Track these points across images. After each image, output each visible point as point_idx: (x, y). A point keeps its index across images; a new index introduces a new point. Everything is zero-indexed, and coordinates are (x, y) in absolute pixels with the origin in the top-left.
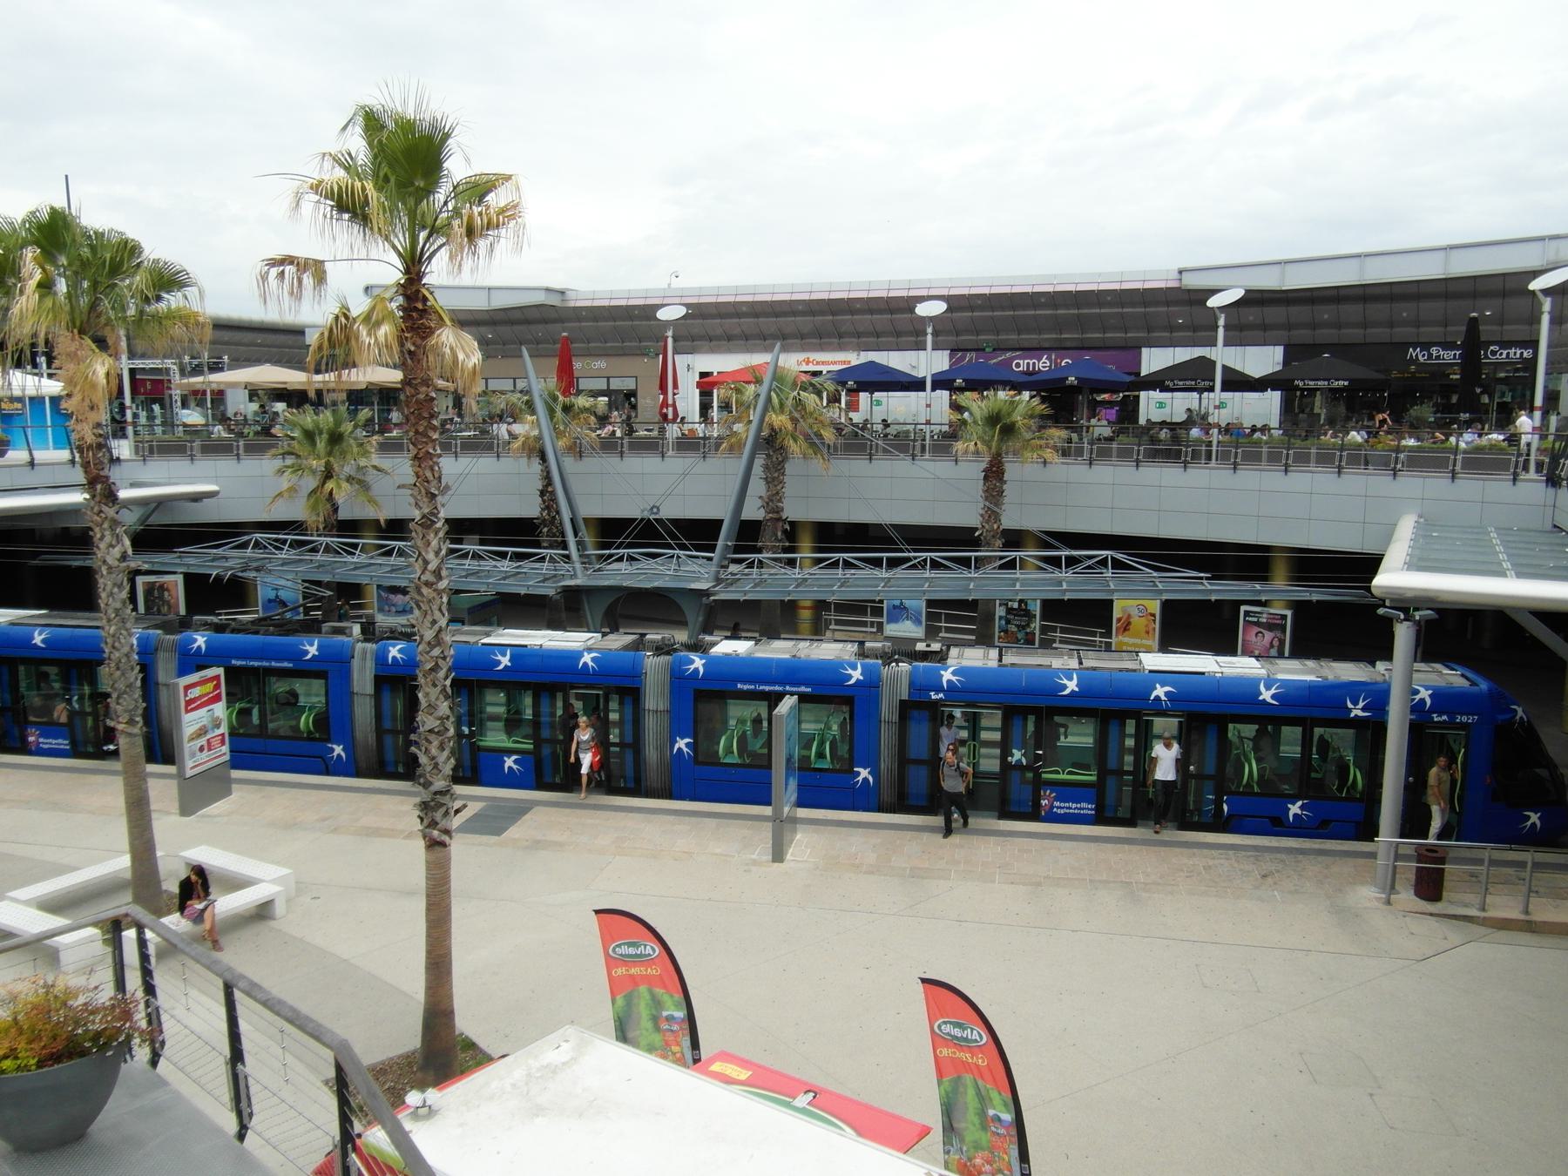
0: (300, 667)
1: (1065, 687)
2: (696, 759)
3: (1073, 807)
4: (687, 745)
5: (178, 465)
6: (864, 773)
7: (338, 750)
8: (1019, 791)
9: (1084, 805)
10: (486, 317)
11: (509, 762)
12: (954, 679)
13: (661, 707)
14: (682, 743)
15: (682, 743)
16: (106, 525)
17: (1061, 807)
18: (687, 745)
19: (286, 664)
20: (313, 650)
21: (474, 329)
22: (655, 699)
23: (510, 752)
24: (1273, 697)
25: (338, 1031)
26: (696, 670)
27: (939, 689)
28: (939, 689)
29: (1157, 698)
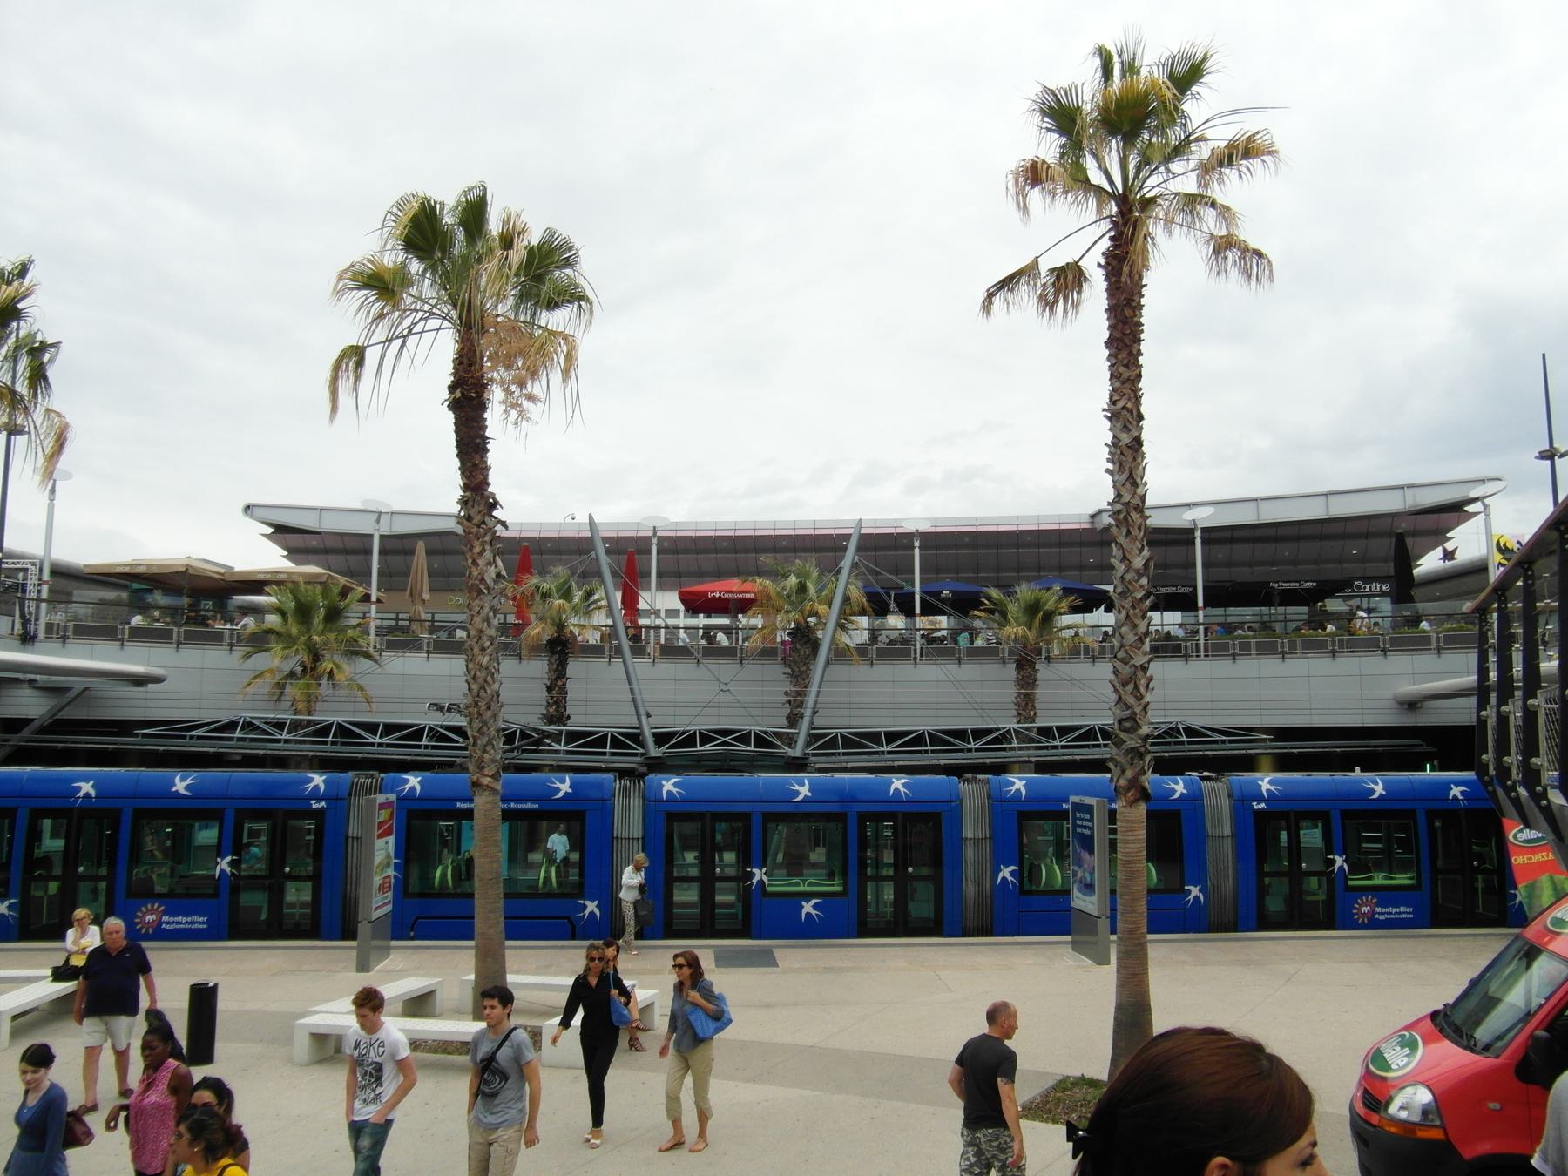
0: (548, 806)
1: (798, 793)
2: (1022, 891)
3: (1394, 912)
4: (1012, 873)
5: (110, 647)
6: (1195, 891)
7: (592, 906)
8: (980, 871)
9: (1403, 909)
10: (338, 544)
11: (808, 907)
12: (675, 790)
13: (979, 835)
14: (1006, 872)
15: (1006, 872)
16: (487, 538)
17: (1383, 913)
18: (1012, 873)
19: (529, 805)
20: (804, 791)
21: (322, 557)
22: (973, 827)
23: (808, 896)
24: (187, 788)
25: (465, 1141)
26: (317, 787)
27: (1260, 799)
28: (1260, 799)
29: (1455, 797)
